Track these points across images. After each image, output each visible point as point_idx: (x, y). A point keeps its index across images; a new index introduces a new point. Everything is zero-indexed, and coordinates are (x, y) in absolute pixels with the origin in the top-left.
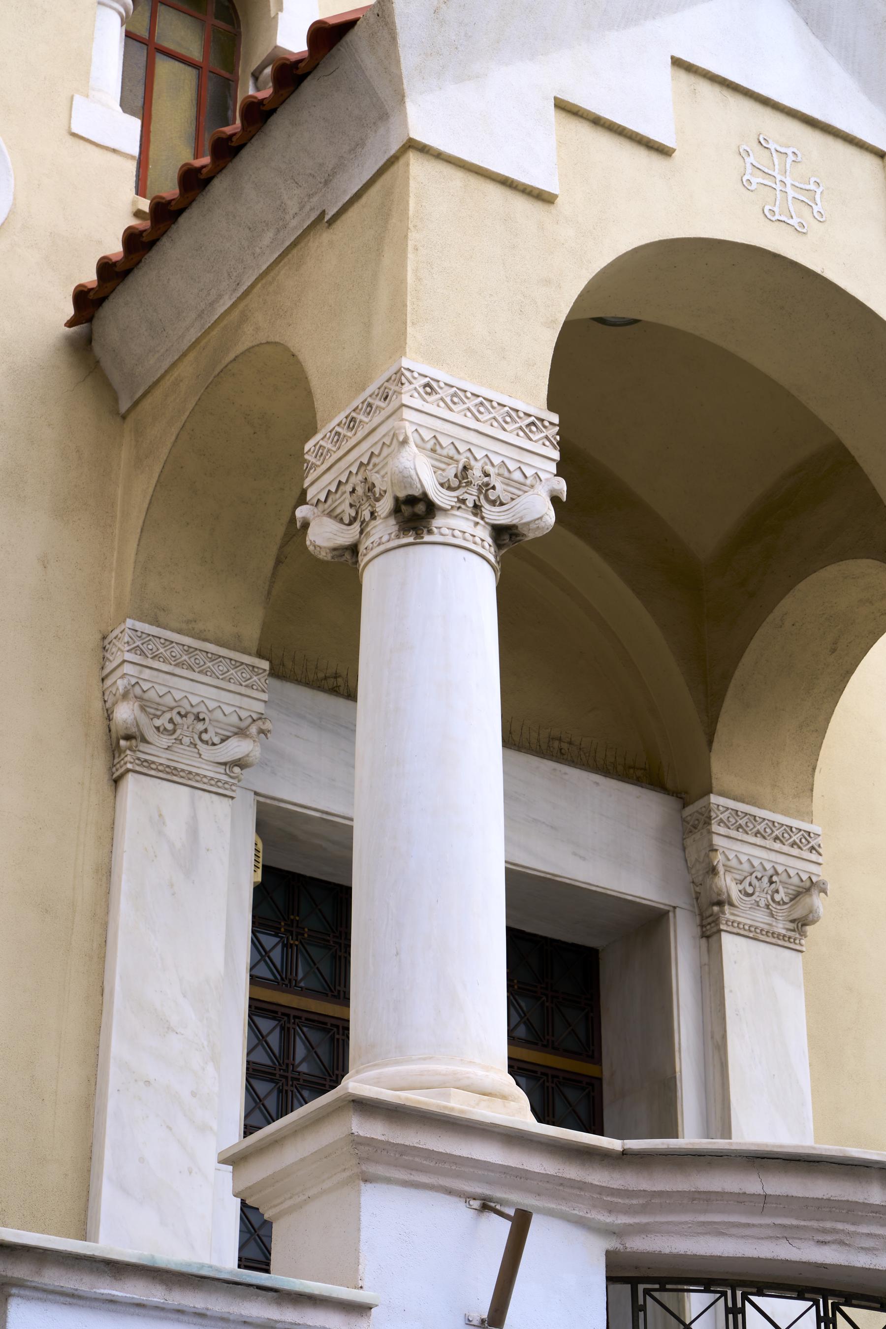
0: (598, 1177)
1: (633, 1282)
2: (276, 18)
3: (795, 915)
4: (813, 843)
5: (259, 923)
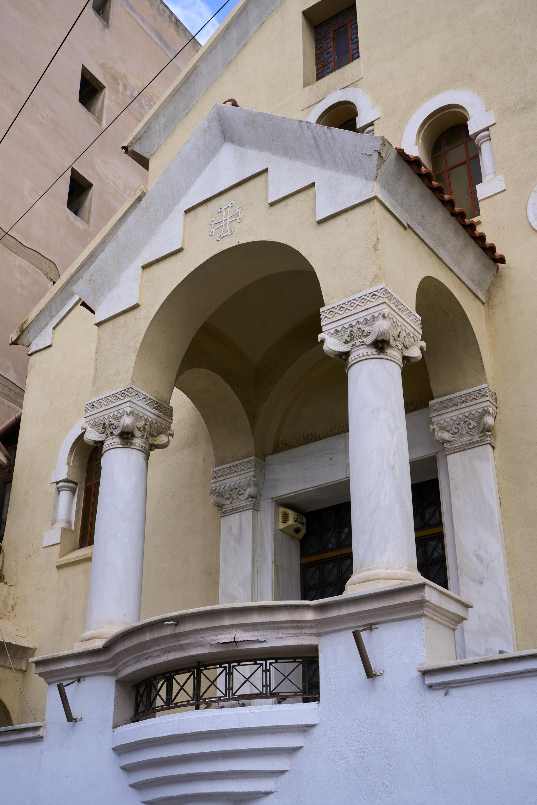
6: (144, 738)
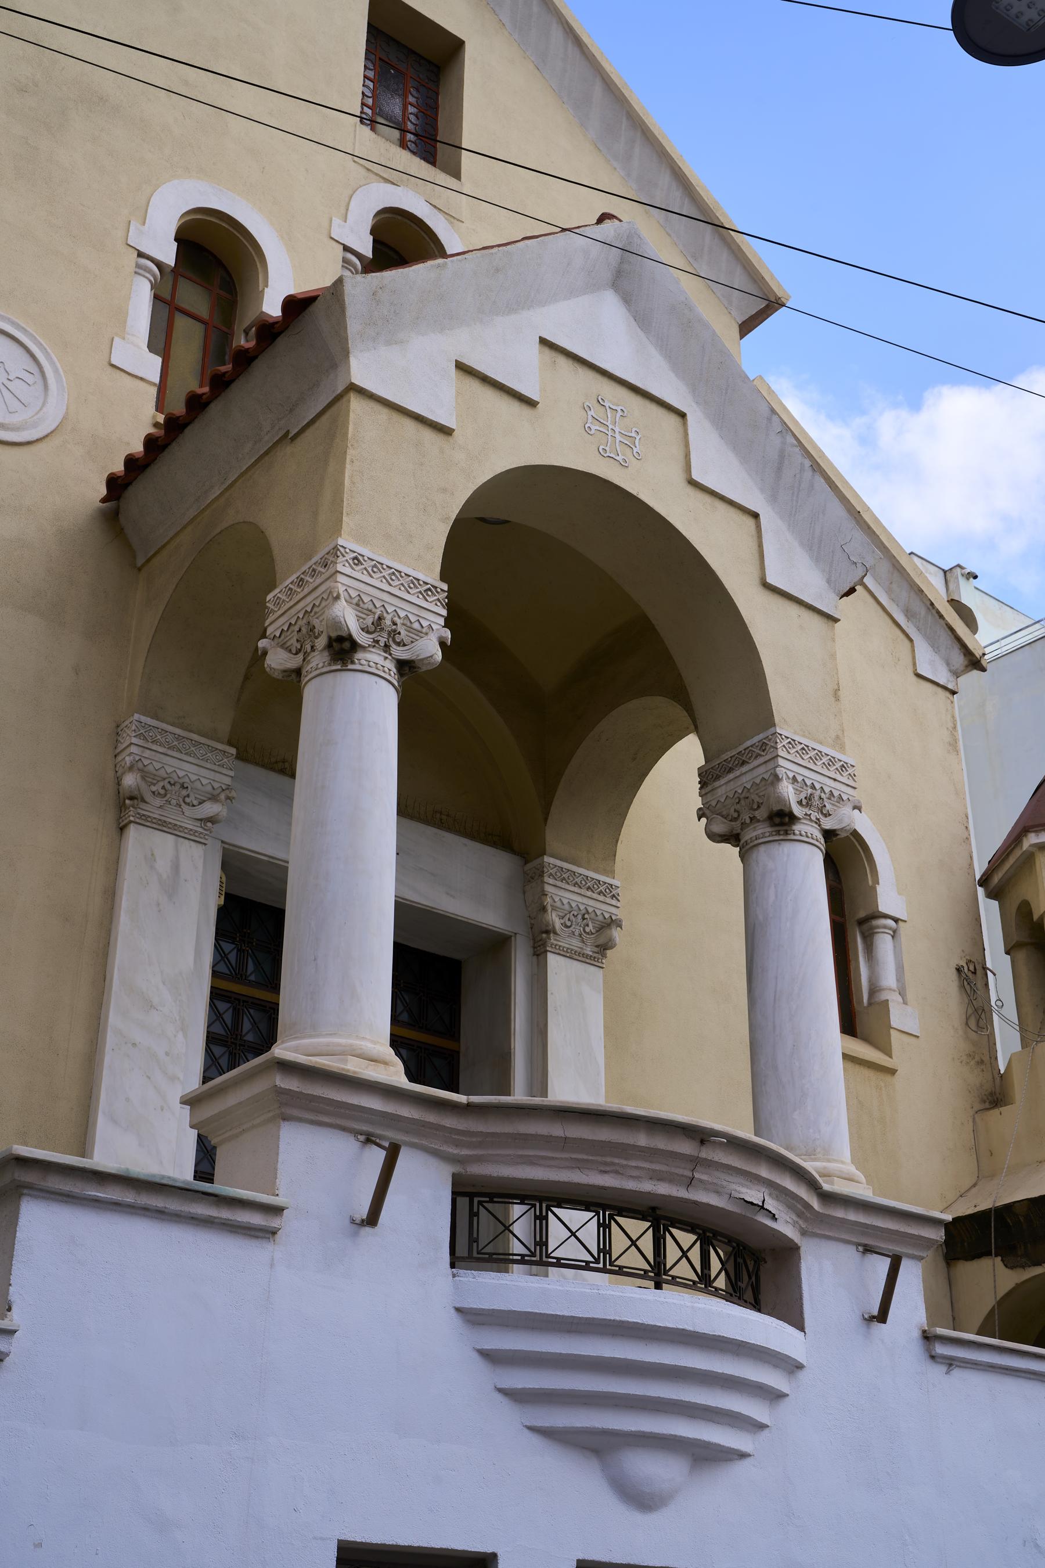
0: (449, 1122)
1: (471, 1196)
2: (263, 291)
3: (599, 942)
4: (614, 892)
5: (221, 934)
6: (618, 1318)
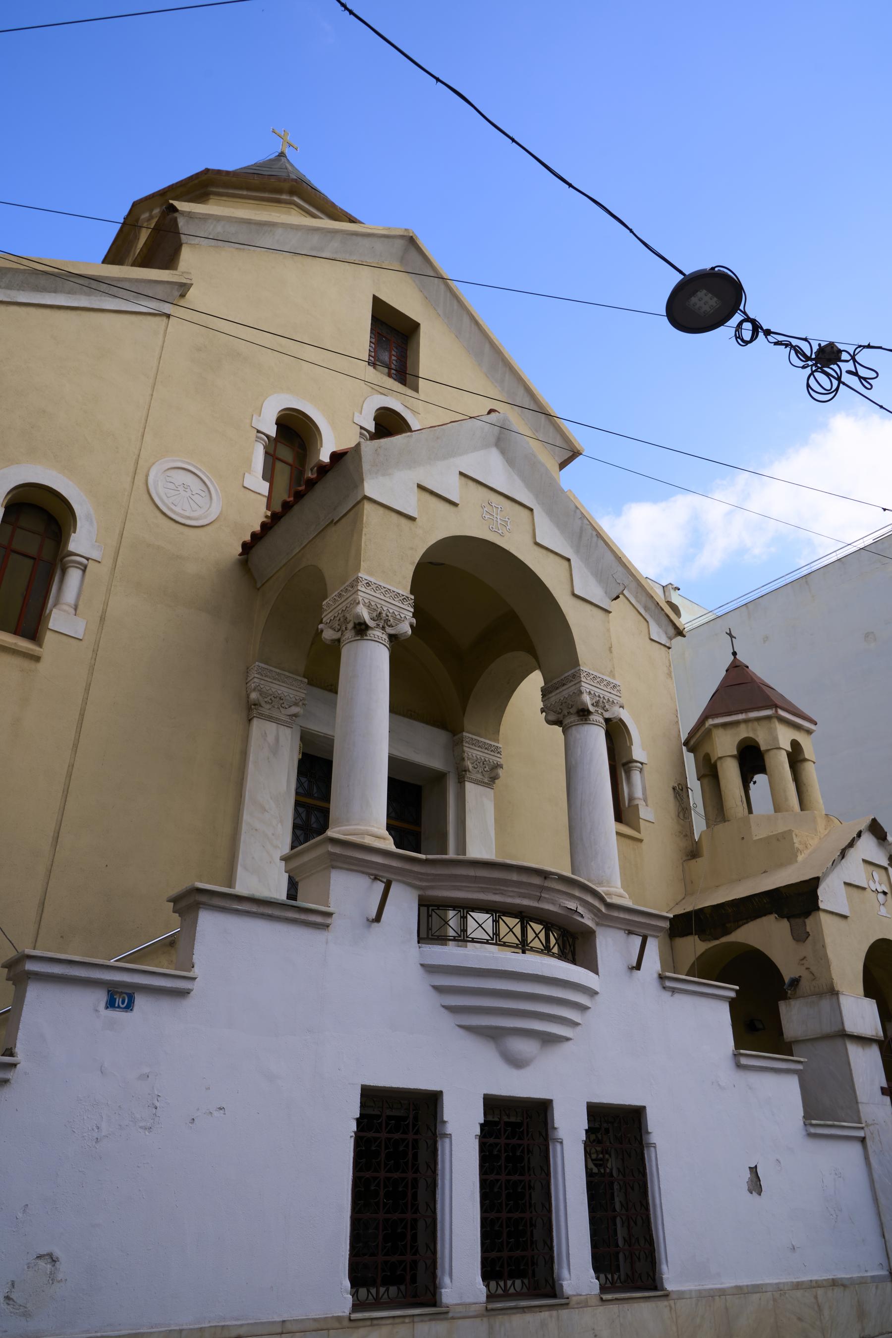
0: (417, 868)
